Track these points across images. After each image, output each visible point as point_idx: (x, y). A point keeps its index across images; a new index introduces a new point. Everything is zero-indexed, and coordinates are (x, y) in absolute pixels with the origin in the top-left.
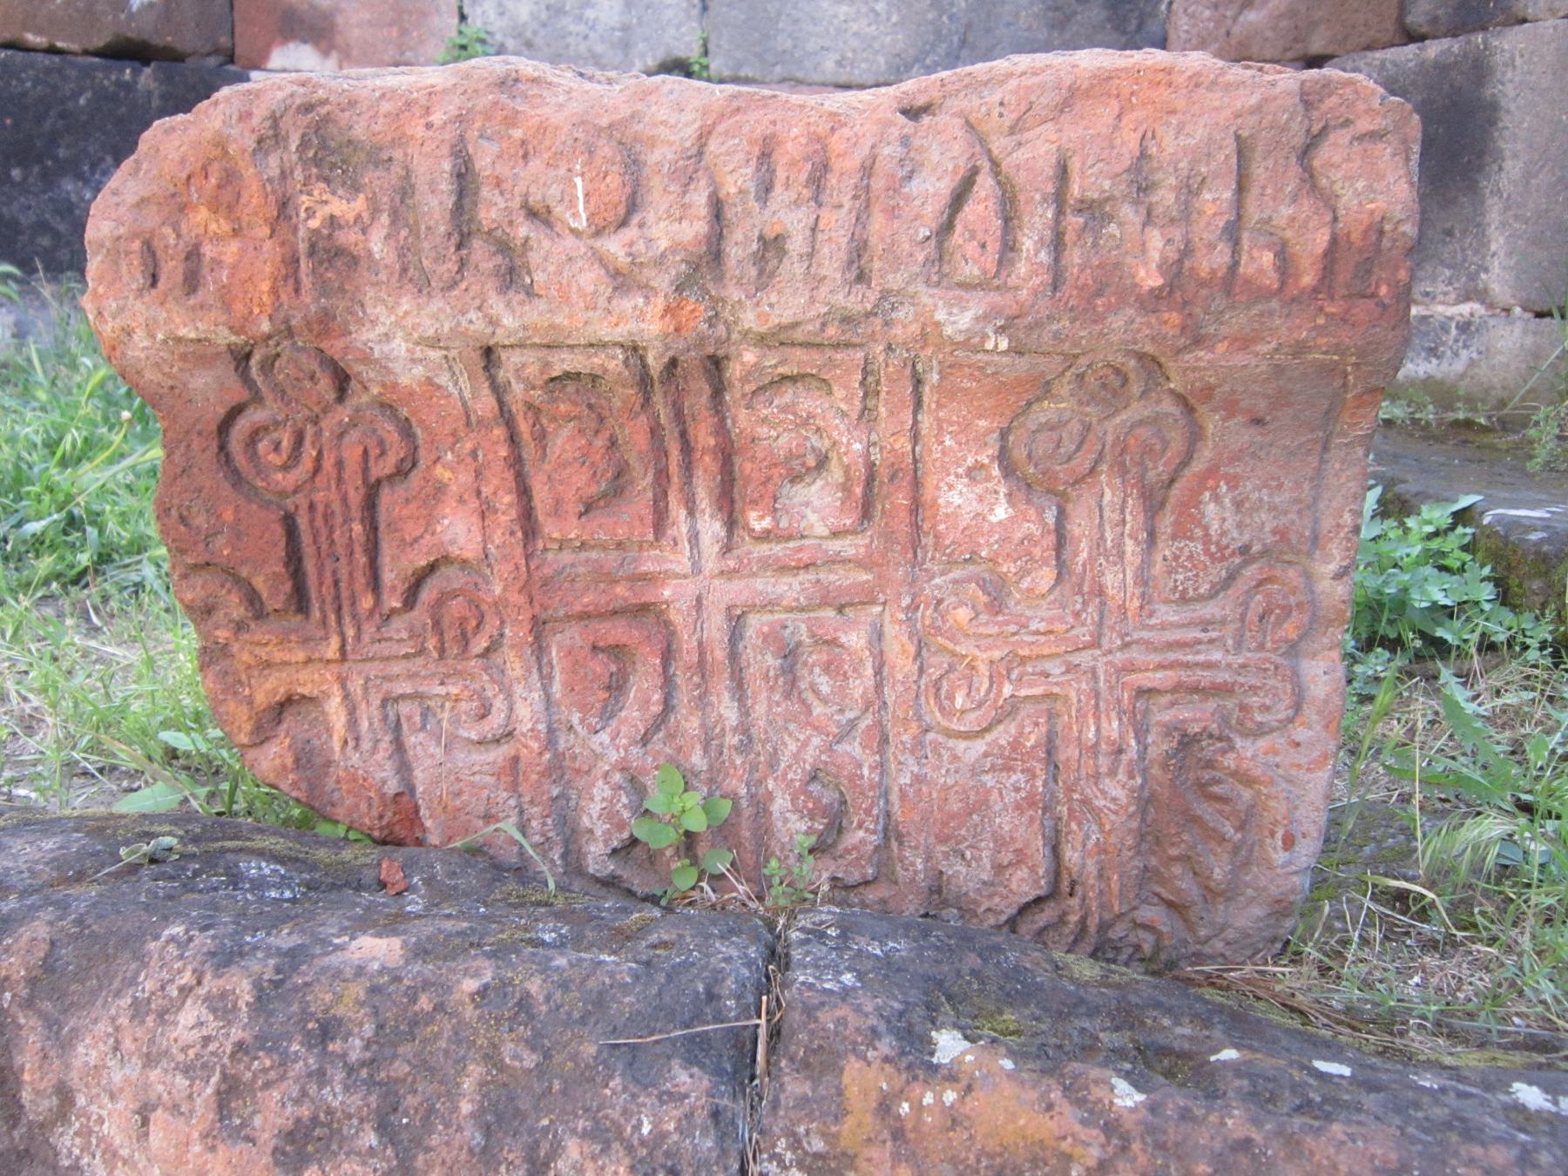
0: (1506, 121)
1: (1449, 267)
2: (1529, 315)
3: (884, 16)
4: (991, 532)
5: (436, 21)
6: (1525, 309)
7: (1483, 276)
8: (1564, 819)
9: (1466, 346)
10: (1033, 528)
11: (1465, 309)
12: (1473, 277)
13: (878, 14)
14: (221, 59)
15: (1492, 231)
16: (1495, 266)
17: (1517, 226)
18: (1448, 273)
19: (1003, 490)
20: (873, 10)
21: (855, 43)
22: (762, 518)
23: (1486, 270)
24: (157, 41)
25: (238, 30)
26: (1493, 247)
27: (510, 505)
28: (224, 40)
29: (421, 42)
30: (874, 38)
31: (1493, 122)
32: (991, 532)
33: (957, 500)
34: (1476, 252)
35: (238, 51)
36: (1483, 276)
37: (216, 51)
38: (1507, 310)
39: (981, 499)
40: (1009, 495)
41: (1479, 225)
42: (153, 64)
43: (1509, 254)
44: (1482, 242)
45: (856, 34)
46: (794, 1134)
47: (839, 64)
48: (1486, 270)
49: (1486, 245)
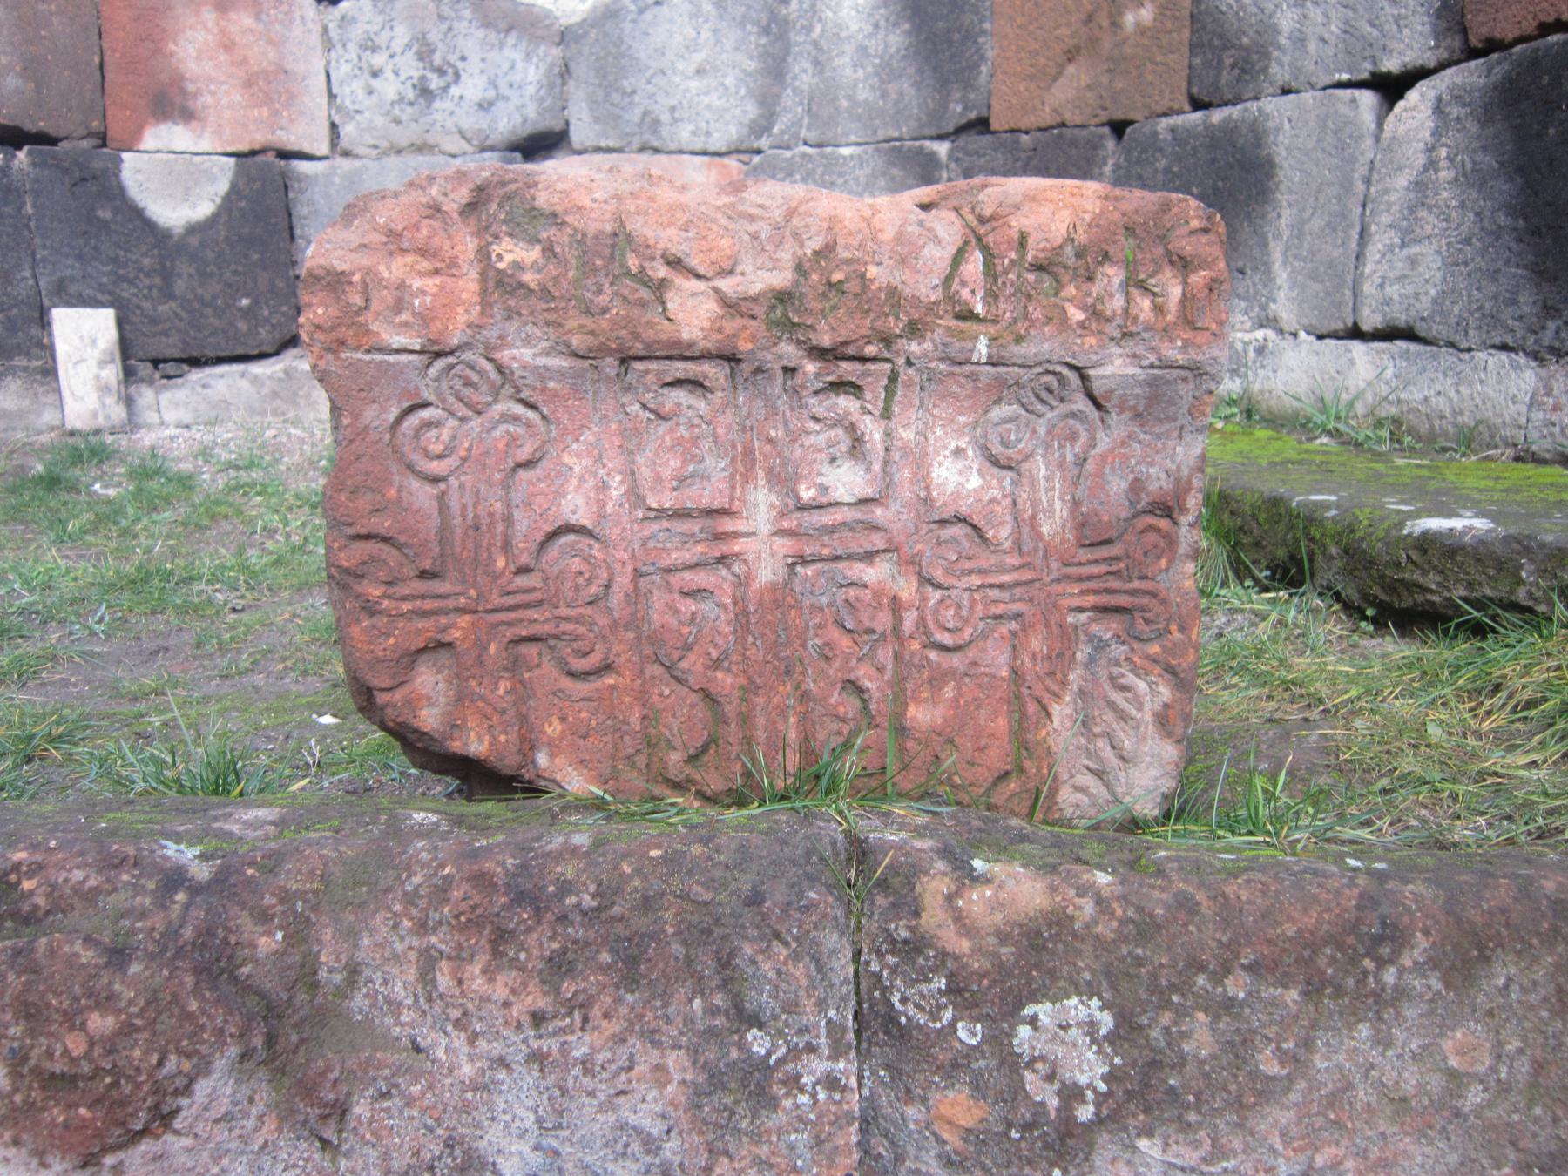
0: (1281, 175)
1: (1246, 299)
2: (1312, 338)
3: (733, 89)
4: (968, 496)
5: (1235, 116)
6: (1308, 333)
7: (1272, 306)
8: (1567, 410)
9: (1263, 366)
10: (997, 494)
11: (1260, 334)
12: (1263, 308)
13: (726, 88)
14: (95, 142)
15: (1277, 266)
16: (1281, 295)
17: (1296, 264)
18: (1243, 304)
19: (976, 466)
20: (722, 84)
21: (708, 115)
22: (808, 489)
23: (1275, 301)
24: (29, 127)
25: (110, 113)
26: (1279, 281)
27: (622, 482)
28: (95, 124)
29: (292, 121)
30: (725, 110)
31: (1270, 175)
32: (968, 496)
33: (945, 474)
34: (1265, 286)
35: (109, 134)
36: (1272, 306)
37: (89, 135)
38: (1295, 335)
39: (960, 473)
40: (979, 470)
41: (1265, 264)
42: (26, 148)
43: (1291, 288)
44: (1269, 279)
45: (708, 107)
46: (887, 930)
47: (694, 133)
48: (1275, 301)
49: (1274, 279)
